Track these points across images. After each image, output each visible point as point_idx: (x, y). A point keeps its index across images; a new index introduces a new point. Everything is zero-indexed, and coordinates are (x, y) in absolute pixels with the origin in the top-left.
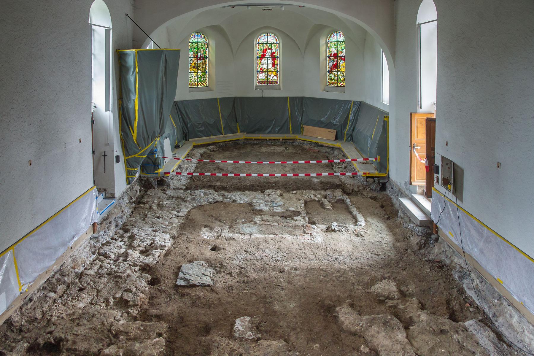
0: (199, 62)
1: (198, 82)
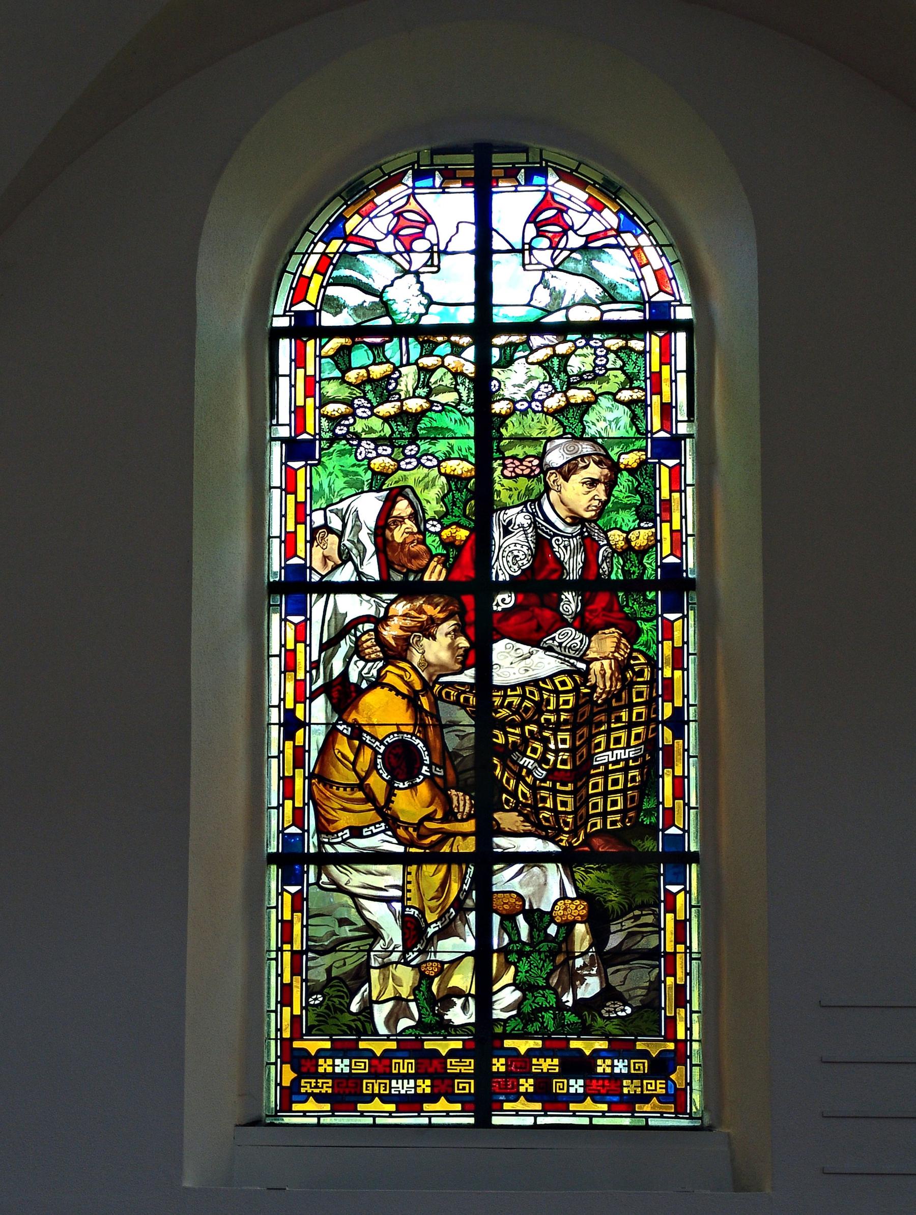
0: (511, 662)
1: (485, 1037)
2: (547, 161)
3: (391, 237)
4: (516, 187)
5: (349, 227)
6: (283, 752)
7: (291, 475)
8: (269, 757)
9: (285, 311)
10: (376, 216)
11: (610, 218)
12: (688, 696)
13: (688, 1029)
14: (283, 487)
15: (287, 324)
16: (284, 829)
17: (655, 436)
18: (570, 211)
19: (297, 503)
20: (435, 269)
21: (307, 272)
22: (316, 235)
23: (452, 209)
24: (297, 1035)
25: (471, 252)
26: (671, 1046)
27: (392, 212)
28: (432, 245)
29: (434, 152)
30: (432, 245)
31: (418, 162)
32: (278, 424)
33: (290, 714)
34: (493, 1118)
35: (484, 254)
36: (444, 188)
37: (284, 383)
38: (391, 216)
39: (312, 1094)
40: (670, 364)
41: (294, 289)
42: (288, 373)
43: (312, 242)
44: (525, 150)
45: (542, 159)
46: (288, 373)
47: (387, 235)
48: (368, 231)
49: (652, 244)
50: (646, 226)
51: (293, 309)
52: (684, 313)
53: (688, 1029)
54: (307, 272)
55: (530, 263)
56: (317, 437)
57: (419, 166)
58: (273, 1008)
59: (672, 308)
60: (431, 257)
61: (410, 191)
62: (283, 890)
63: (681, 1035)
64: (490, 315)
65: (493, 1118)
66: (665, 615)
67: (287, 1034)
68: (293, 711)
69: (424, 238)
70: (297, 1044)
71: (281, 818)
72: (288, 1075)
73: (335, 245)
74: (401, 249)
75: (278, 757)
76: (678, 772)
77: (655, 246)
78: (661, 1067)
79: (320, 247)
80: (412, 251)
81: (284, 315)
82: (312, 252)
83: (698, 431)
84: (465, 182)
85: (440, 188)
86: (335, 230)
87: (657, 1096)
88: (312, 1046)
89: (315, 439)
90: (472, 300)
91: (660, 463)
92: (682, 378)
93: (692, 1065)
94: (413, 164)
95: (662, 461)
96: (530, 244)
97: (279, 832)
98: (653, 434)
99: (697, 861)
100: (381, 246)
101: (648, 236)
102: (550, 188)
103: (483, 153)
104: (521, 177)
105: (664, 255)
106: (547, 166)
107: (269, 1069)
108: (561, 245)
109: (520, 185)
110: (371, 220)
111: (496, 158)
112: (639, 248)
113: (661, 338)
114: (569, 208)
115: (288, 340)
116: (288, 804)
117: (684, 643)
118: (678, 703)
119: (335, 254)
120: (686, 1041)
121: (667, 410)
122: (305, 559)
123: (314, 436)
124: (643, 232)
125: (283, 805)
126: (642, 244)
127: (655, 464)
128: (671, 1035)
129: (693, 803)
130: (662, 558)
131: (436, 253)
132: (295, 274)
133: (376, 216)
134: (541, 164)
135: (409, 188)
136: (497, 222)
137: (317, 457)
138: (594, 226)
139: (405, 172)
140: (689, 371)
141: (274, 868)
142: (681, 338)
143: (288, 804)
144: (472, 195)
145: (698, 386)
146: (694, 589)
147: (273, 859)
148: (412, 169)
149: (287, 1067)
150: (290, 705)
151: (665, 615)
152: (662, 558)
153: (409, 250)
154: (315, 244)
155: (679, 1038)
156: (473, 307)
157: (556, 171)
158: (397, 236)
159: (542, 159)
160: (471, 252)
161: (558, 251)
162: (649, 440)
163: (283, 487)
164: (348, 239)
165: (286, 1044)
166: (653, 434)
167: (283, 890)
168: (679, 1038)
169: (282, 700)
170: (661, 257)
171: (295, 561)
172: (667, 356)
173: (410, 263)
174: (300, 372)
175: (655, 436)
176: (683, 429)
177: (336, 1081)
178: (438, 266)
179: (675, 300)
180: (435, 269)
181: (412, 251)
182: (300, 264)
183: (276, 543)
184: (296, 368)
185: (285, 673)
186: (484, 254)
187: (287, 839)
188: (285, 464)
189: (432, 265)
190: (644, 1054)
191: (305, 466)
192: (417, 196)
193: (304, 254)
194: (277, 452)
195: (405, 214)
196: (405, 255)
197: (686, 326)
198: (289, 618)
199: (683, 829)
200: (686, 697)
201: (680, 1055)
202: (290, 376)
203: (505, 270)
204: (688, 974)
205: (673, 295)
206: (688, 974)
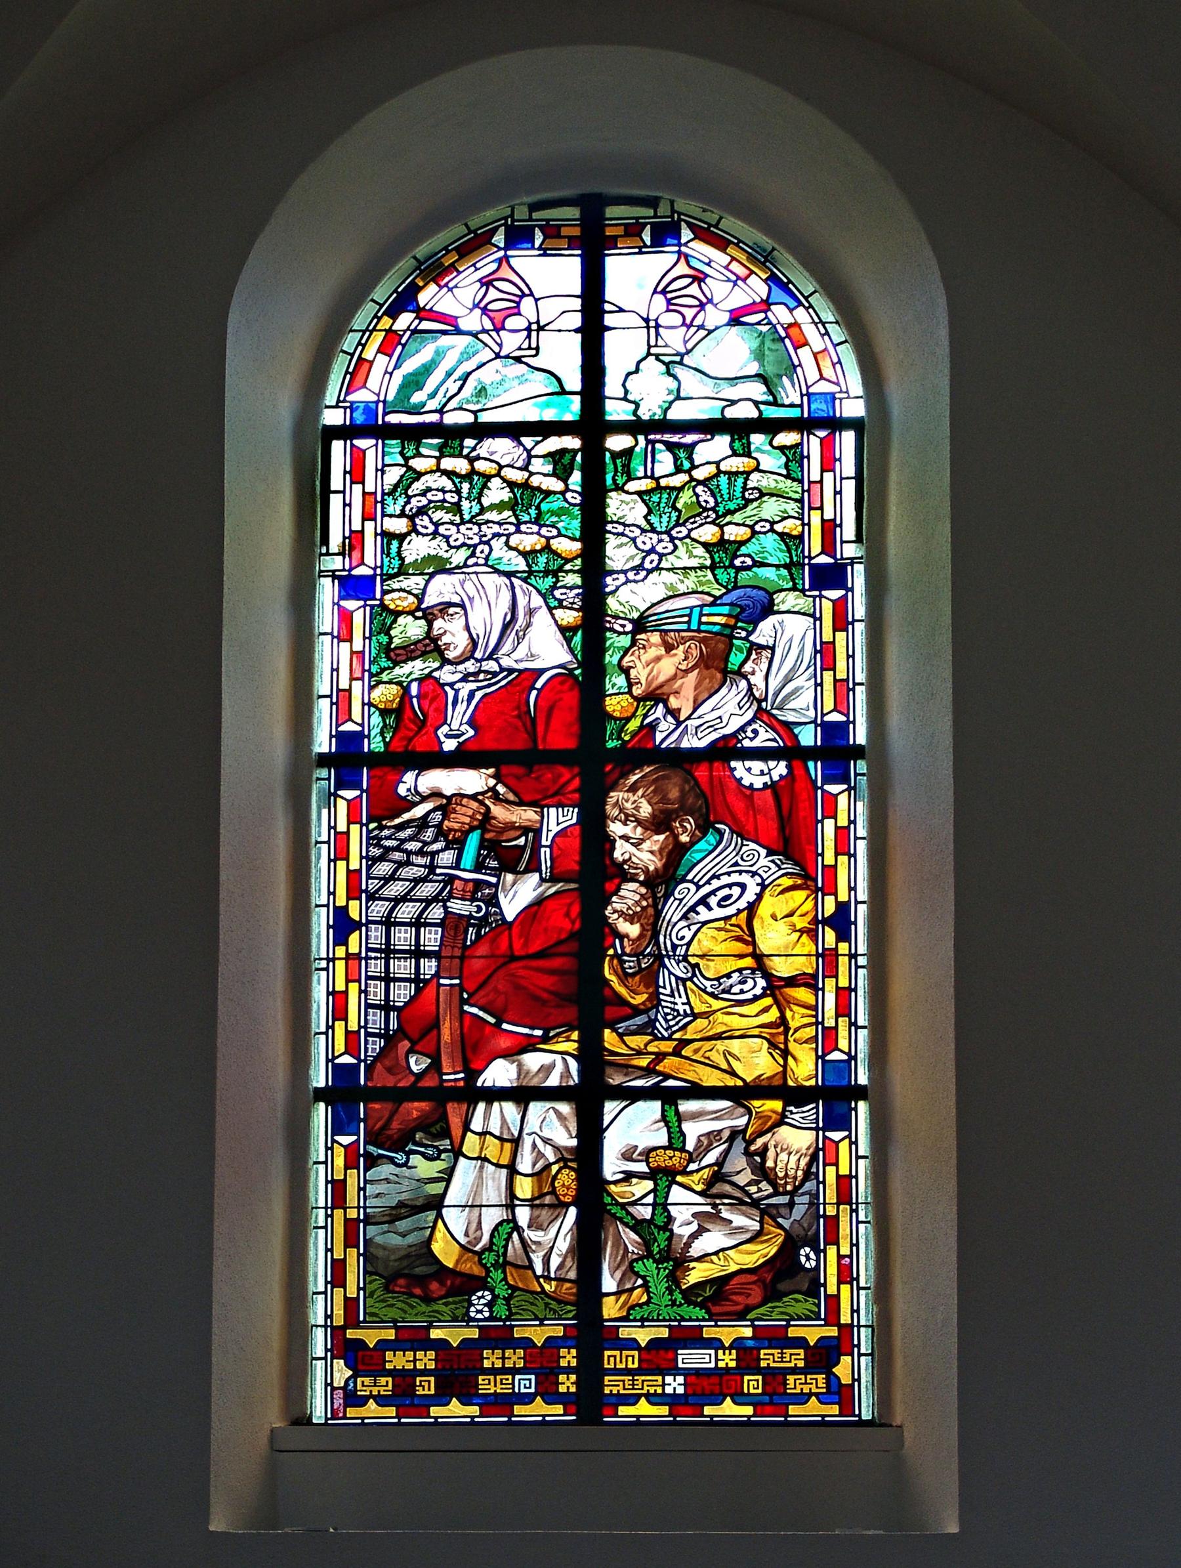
2: (680, 214)
3: (478, 312)
4: (640, 248)
5: (423, 298)
6: (327, 1148)
7: (346, 618)
8: (317, 842)
9: (338, 401)
10: (456, 286)
11: (758, 287)
12: (855, 889)
13: (855, 1311)
14: (336, 634)
15: (340, 422)
16: (334, 1058)
17: (813, 562)
18: (708, 280)
19: (349, 871)
20: (534, 352)
21: (354, 988)
22: (381, 306)
23: (555, 275)
24: (352, 1320)
25: (576, 331)
26: (833, 1332)
27: (480, 280)
28: (530, 324)
29: (534, 207)
30: (530, 324)
31: (512, 216)
32: (328, 554)
33: (341, 913)
34: (577, 216)
35: (593, 333)
36: (545, 250)
37: (336, 501)
38: (478, 285)
39: (371, 1396)
40: (833, 470)
41: (349, 473)
42: (341, 489)
43: (375, 316)
44: (653, 203)
45: (673, 211)
46: (341, 489)
47: (471, 310)
48: (446, 304)
49: (814, 322)
50: (806, 298)
51: (348, 398)
52: (854, 409)
53: (855, 1311)
54: (354, 988)
55: (656, 346)
56: (378, 571)
57: (513, 221)
58: (321, 1288)
59: (837, 402)
60: (529, 336)
61: (501, 253)
62: (333, 1141)
63: (845, 1318)
64: (601, 411)
65: (577, 216)
66: (826, 787)
67: (339, 1321)
68: (345, 909)
69: (519, 314)
70: (351, 1334)
71: (331, 1045)
72: (342, 1373)
73: (405, 320)
74: (488, 325)
75: (326, 1033)
76: (844, 983)
77: (816, 324)
78: (822, 1357)
79: (386, 322)
80: (503, 328)
81: (337, 406)
82: (374, 329)
83: (867, 554)
84: (572, 243)
85: (540, 248)
86: (405, 300)
87: (817, 1395)
88: (371, 1337)
89: (375, 575)
90: (578, 292)
91: (821, 596)
92: (849, 488)
93: (860, 1355)
94: (506, 218)
95: (824, 593)
96: (656, 321)
97: (328, 1061)
98: (810, 558)
99: (865, 1098)
100: (464, 325)
101: (807, 309)
102: (684, 249)
103: (592, 208)
104: (647, 237)
105: (827, 333)
106: (680, 220)
107: (316, 1234)
108: (697, 322)
109: (646, 246)
110: (450, 290)
111: (611, 211)
112: (796, 325)
113: (822, 439)
114: (707, 276)
115: (342, 442)
116: (339, 1026)
117: (850, 822)
118: (843, 896)
119: (405, 331)
120: (851, 1326)
121: (830, 528)
122: (362, 725)
123: (375, 569)
124: (800, 304)
125: (333, 1027)
126: (799, 321)
127: (814, 597)
128: (832, 1317)
129: (862, 1021)
130: (823, 715)
131: (537, 328)
132: (352, 355)
133: (456, 286)
134: (672, 217)
135: (500, 249)
136: (613, 292)
137: (378, 596)
138: (740, 299)
139: (495, 230)
140: (859, 478)
141: (322, 1105)
142: (847, 439)
143: (339, 1026)
144: (579, 259)
145: (869, 510)
146: (863, 758)
147: (320, 1095)
148: (505, 225)
149: (339, 1364)
150: (341, 902)
151: (826, 787)
152: (823, 715)
153: (499, 328)
154: (379, 319)
155: (842, 1322)
156: (604, 1290)
157: (691, 226)
158: (485, 311)
159: (673, 211)
160: (576, 331)
161: (693, 329)
162: (807, 568)
163: (336, 634)
164: (423, 314)
165: (337, 1332)
166: (810, 558)
167: (333, 1141)
168: (842, 1322)
169: (332, 894)
170: (822, 335)
171: (349, 727)
172: (829, 462)
173: (500, 345)
174: (357, 488)
175: (813, 562)
176: (850, 551)
177: (401, 1409)
178: (537, 349)
179: (841, 392)
180: (534, 352)
181: (503, 328)
182: (359, 343)
183: (324, 704)
184: (352, 483)
185: (335, 861)
186: (593, 333)
187: (340, 1072)
188: (338, 604)
189: (530, 348)
190: (801, 1342)
191: (364, 606)
192: (512, 260)
193: (364, 332)
194: (327, 591)
195: (495, 283)
196: (494, 334)
197: (856, 425)
198: (339, 793)
199: (848, 1054)
200: (852, 889)
201: (841, 1344)
202: (343, 492)
203: (621, 348)
204: (855, 1245)
205: (837, 384)
206: (855, 1245)
